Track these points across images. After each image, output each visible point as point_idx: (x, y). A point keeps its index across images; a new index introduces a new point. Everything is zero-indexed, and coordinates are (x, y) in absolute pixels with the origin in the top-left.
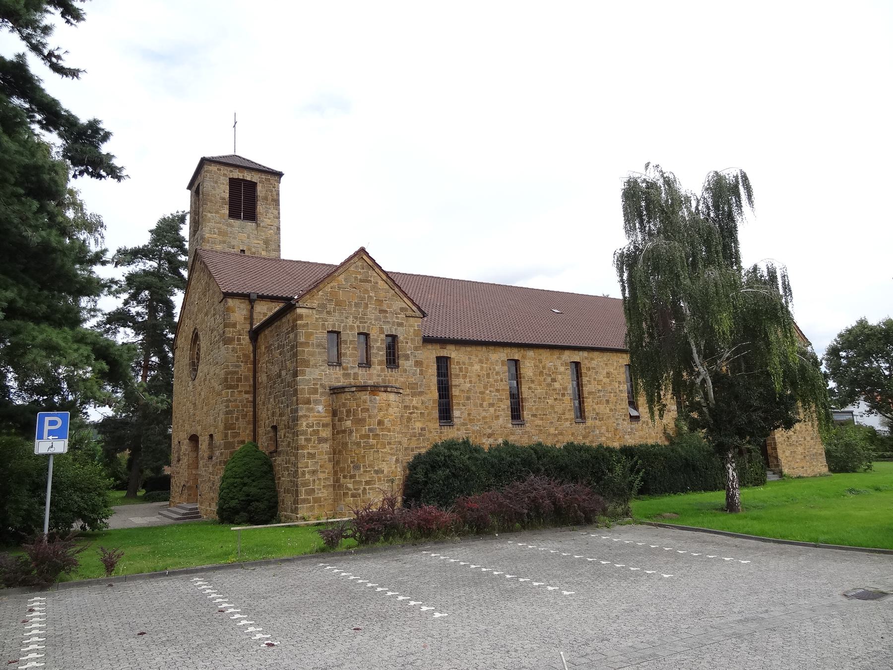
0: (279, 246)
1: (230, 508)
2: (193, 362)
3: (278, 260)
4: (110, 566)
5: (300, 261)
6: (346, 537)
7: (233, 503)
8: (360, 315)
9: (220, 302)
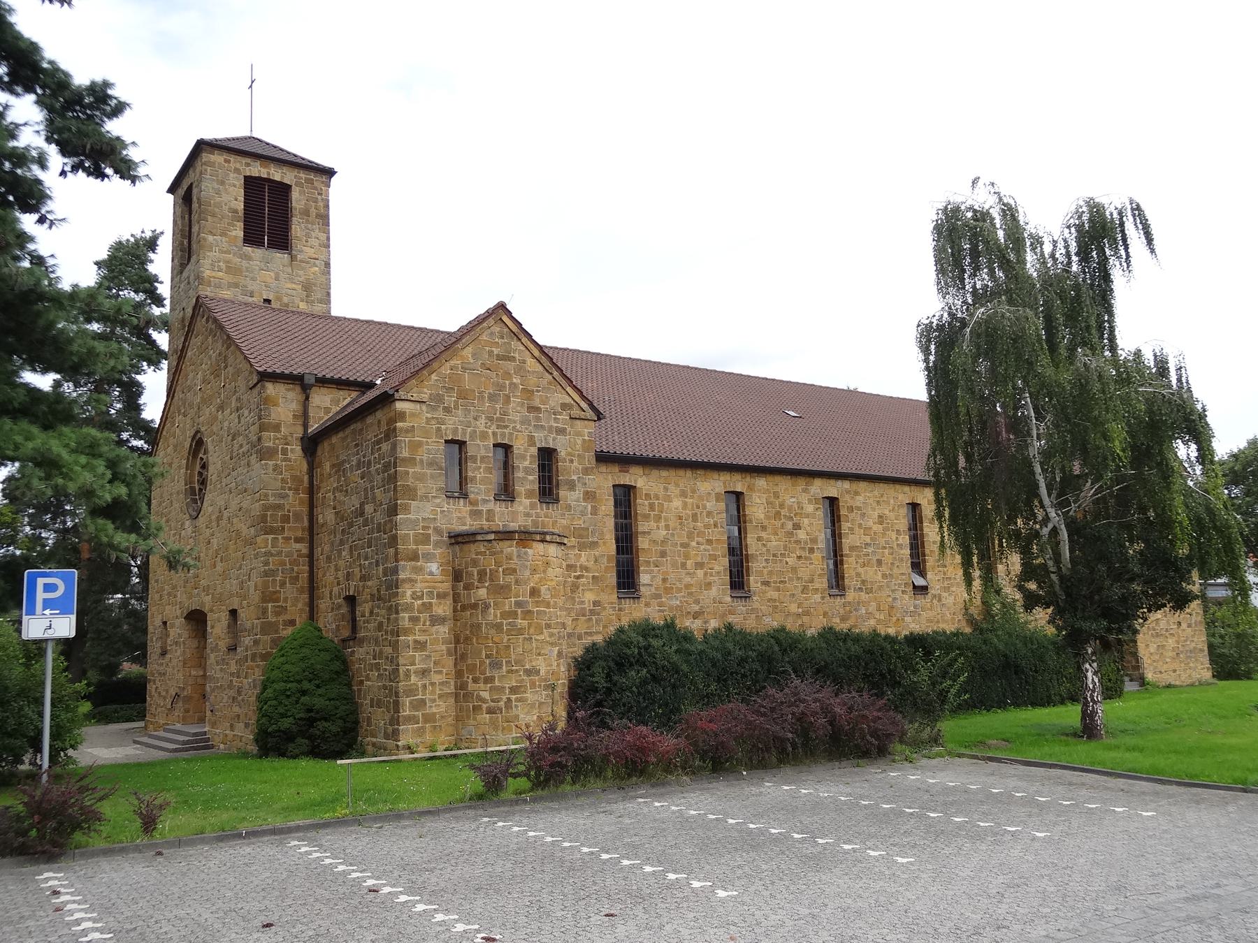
0: (329, 294)
1: (279, 731)
2: (192, 489)
3: (327, 317)
4: (149, 823)
5: (372, 321)
6: (515, 776)
7: (286, 723)
8: (498, 415)
9: (251, 389)
